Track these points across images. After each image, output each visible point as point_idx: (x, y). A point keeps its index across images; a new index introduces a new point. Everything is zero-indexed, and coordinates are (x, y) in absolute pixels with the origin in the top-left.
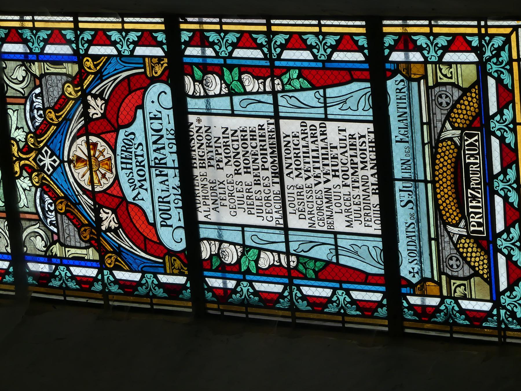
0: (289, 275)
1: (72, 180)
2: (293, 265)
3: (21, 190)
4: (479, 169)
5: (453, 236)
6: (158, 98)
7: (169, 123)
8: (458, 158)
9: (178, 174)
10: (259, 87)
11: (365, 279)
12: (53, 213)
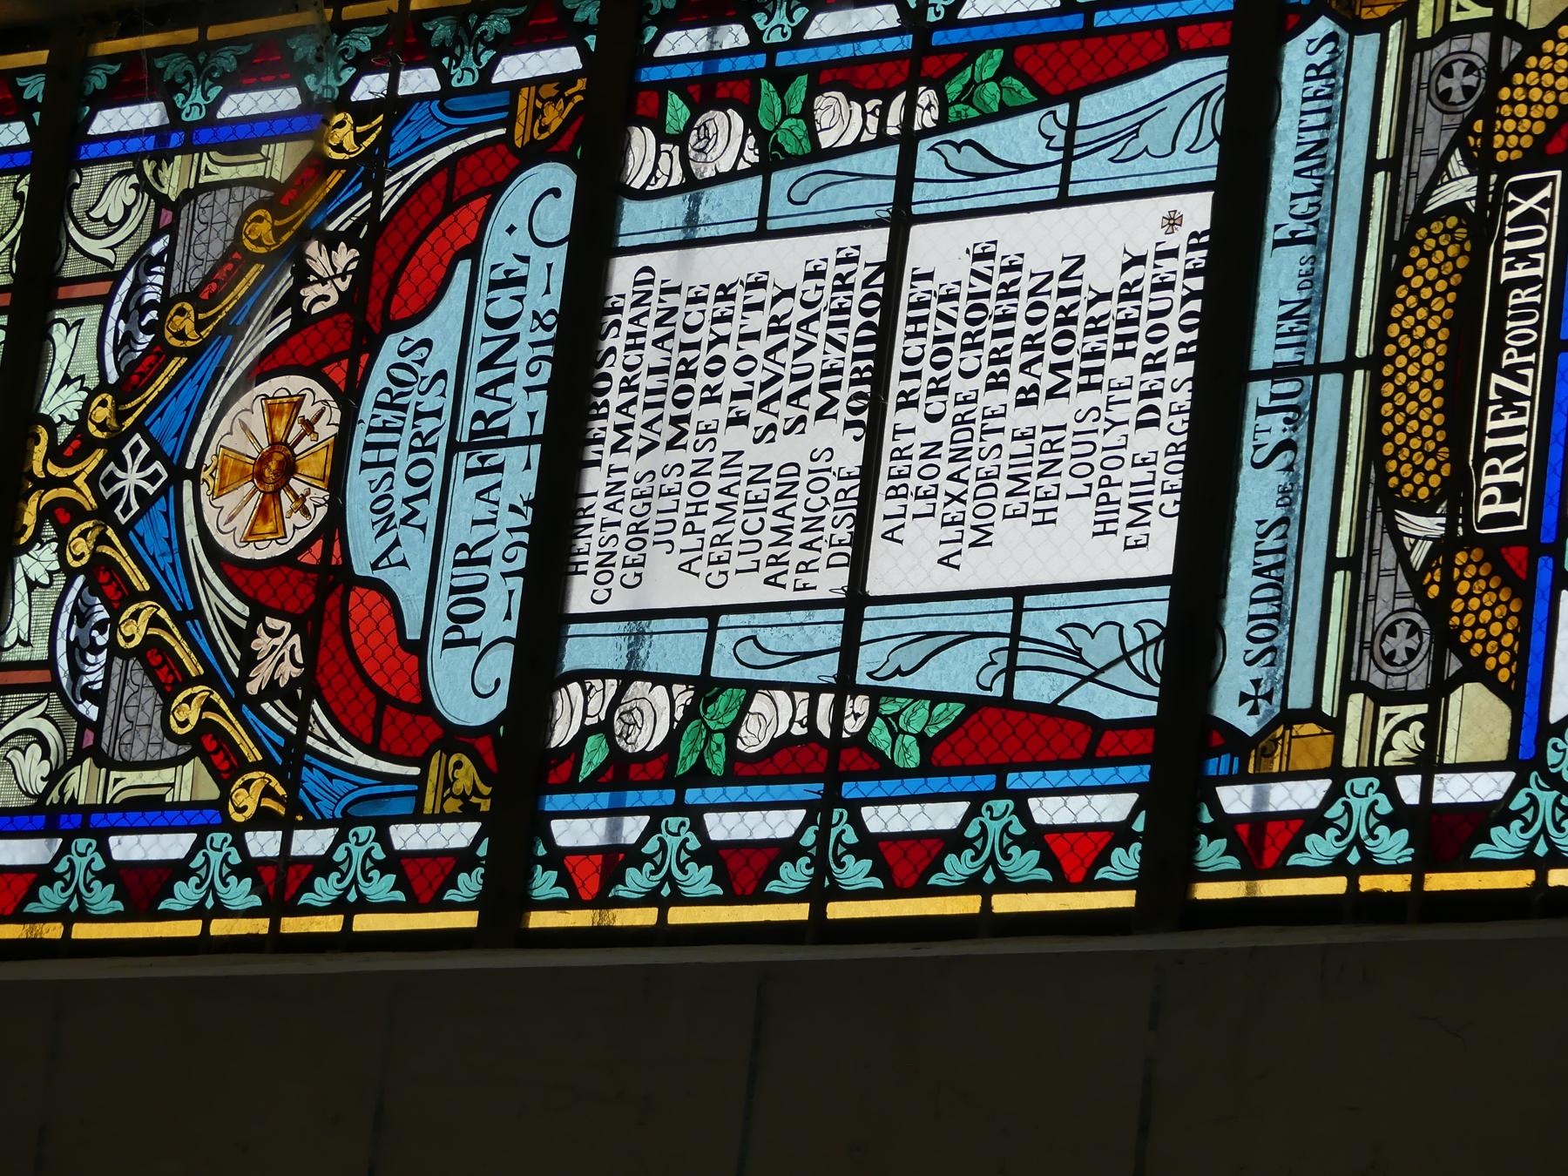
0: (825, 766)
1: (191, 532)
2: (851, 726)
3: (21, 586)
4: (1537, 299)
5: (1413, 546)
6: (540, 202)
7: (548, 291)
8: (1473, 275)
9: (535, 463)
10: (864, 127)
11: (1079, 742)
12: (103, 657)
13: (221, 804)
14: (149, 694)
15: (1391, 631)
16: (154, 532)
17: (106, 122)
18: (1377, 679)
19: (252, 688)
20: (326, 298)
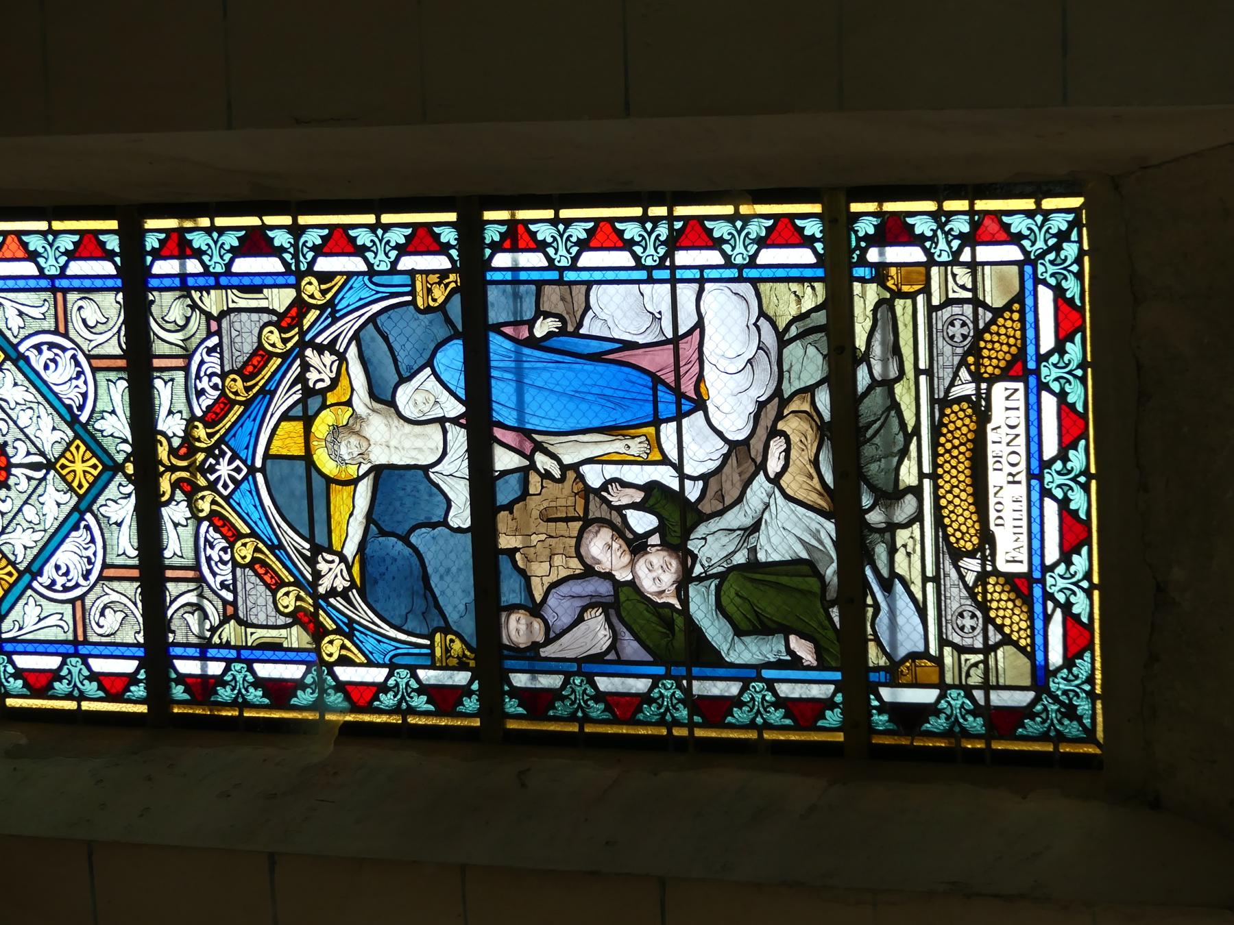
13: (318, 651)
18: (956, 639)
19: (322, 590)
20: (322, 380)
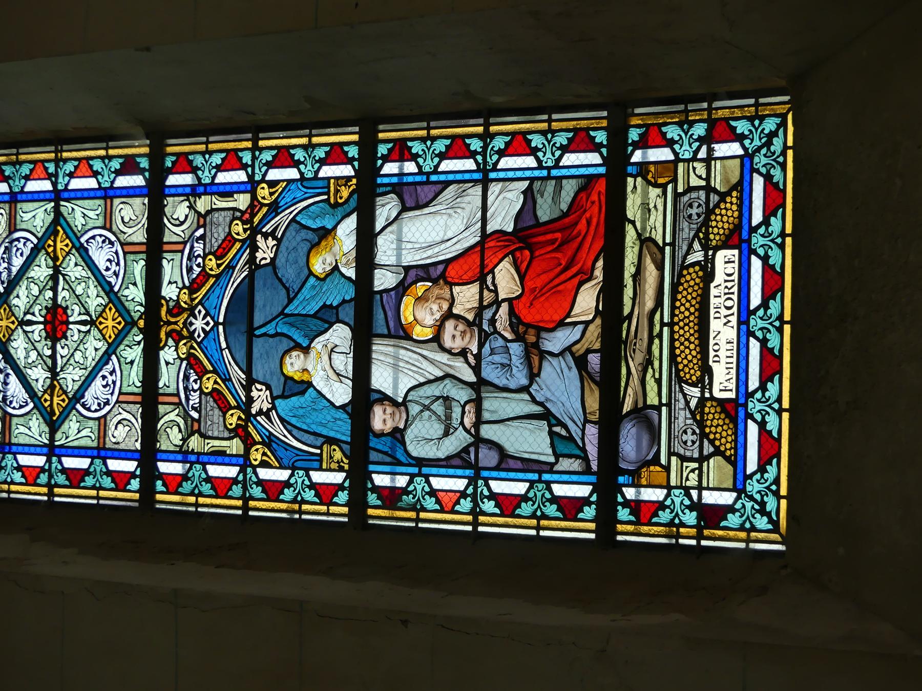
14: (217, 412)
15: (685, 432)
16: (210, 345)
17: (173, 180)
18: (682, 452)
20: (265, 259)
